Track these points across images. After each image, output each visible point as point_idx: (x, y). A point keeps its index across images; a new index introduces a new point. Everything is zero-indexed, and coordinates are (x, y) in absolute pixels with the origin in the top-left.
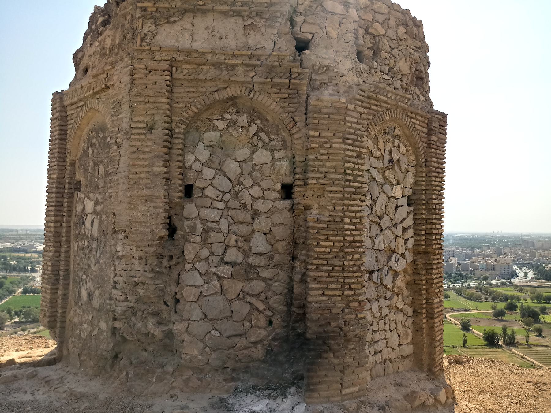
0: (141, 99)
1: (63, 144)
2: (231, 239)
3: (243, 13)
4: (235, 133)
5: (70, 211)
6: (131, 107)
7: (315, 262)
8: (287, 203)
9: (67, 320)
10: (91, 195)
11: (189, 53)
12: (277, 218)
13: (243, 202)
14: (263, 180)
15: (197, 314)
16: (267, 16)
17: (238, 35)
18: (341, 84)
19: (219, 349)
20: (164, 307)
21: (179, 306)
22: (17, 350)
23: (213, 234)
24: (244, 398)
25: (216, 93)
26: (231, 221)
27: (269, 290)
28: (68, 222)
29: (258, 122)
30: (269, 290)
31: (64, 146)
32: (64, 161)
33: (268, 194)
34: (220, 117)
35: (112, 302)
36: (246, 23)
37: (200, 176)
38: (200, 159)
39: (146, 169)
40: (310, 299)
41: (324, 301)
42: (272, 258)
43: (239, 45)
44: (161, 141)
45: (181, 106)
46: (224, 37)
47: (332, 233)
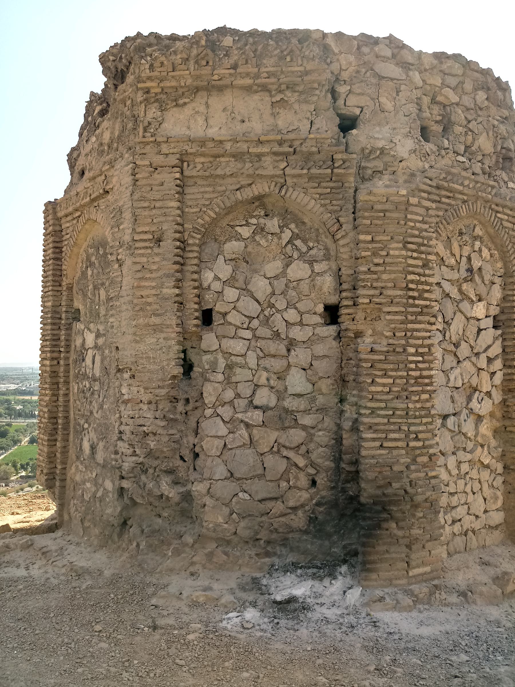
0: (146, 204)
1: (58, 265)
2: (260, 376)
3: (270, 86)
4: (263, 242)
5: (68, 346)
8: (332, 329)
11: (203, 142)
12: (320, 349)
13: (275, 329)
14: (300, 300)
15: (221, 471)
16: (301, 88)
17: (264, 116)
18: (400, 172)
19: (250, 515)
20: (181, 463)
21: (199, 462)
23: (238, 370)
24: (282, 578)
26: (261, 354)
27: (311, 441)
28: (67, 359)
29: (293, 226)
30: (311, 441)
31: (59, 268)
33: (309, 319)
34: (244, 223)
36: (274, 100)
37: (220, 299)
38: (221, 276)
39: (153, 292)
40: (364, 453)
42: (313, 400)
44: (170, 256)
45: (195, 210)
46: (247, 120)
47: (391, 366)
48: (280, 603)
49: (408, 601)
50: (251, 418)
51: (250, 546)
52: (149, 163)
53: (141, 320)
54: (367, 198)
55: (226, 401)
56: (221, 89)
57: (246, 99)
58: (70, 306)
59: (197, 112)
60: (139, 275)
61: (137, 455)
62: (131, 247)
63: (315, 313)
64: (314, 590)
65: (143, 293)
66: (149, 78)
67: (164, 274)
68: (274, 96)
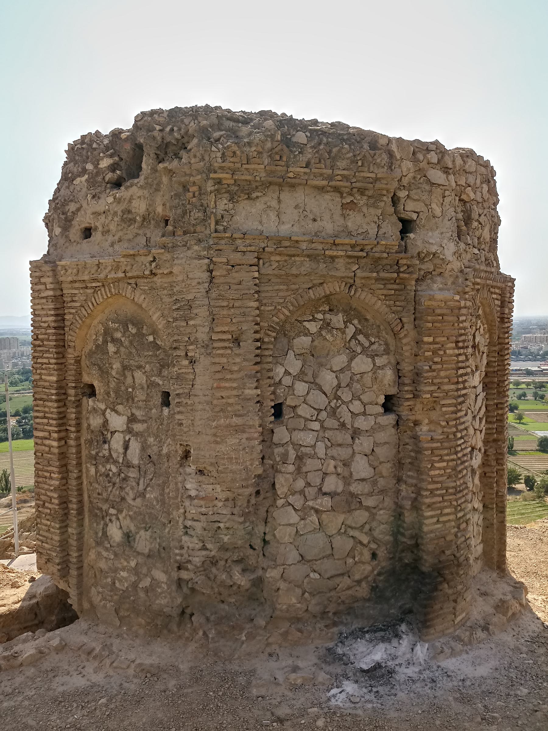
0: (225, 304)
1: (60, 334)
2: (328, 465)
5: (78, 425)
6: (211, 313)
7: (430, 487)
8: (391, 418)
9: (85, 565)
10: (120, 408)
11: (279, 241)
12: (382, 437)
13: (342, 420)
14: (364, 392)
15: (293, 556)
16: (370, 193)
17: (334, 216)
19: (319, 593)
20: (251, 551)
21: (270, 549)
23: (309, 461)
24: (354, 645)
25: (310, 291)
26: (329, 444)
27: (374, 519)
28: (78, 439)
29: (356, 322)
31: (62, 337)
33: (371, 409)
34: (311, 318)
36: (344, 201)
37: (290, 393)
38: (291, 371)
39: (235, 392)
40: (425, 529)
43: (337, 228)
44: (252, 356)
45: (270, 308)
46: (319, 219)
47: (446, 452)
48: (367, 671)
49: (459, 647)
50: (321, 505)
51: (318, 619)
52: (225, 260)
56: (293, 186)
57: (318, 197)
58: (78, 380)
59: (269, 207)
61: (207, 549)
62: (207, 346)
64: (388, 652)
65: (223, 394)
67: (246, 375)
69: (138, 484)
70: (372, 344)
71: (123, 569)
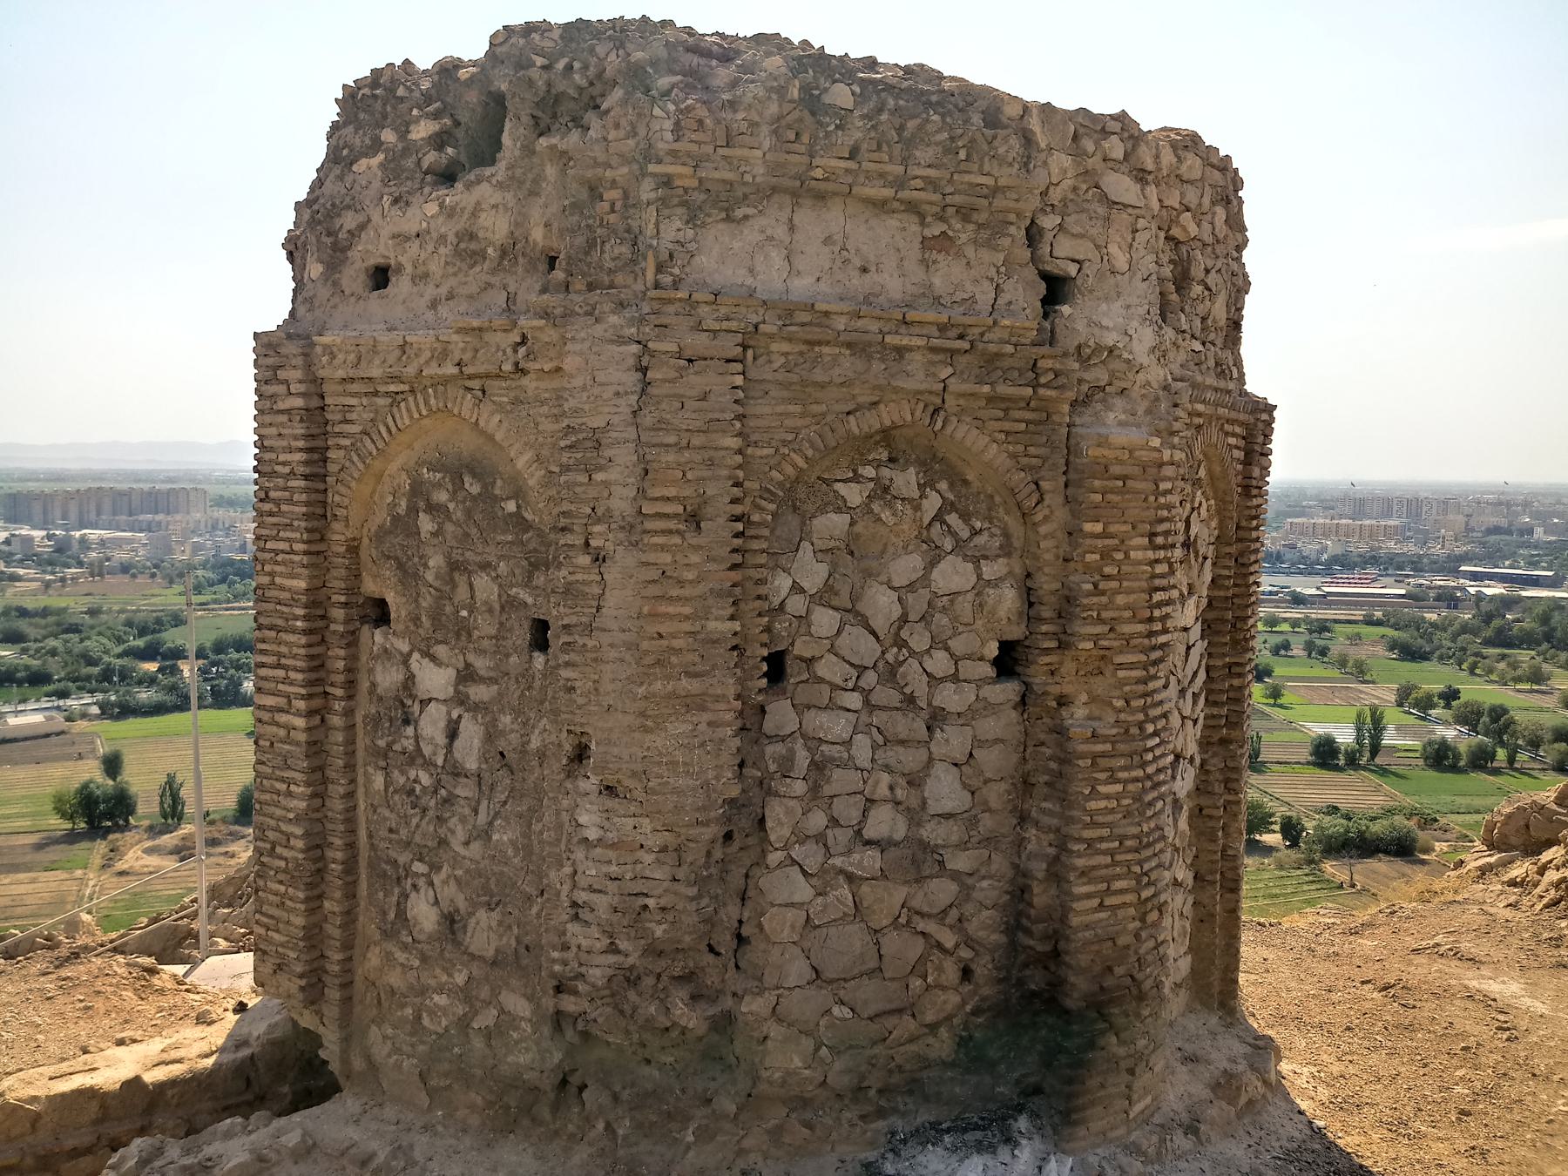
0: (672, 439)
1: (317, 491)
2: (877, 783)
3: (927, 207)
4: (886, 515)
5: (351, 684)
6: (642, 459)
7: (1087, 834)
8: (1008, 691)
9: (358, 979)
10: (441, 651)
11: (788, 312)
12: (990, 727)
13: (907, 690)
14: (956, 634)
15: (798, 970)
16: (982, 217)
17: (906, 263)
18: (1136, 392)
19: (851, 1047)
20: (711, 958)
21: (750, 955)
22: (121, 1043)
24: (920, 1158)
25: (851, 418)
26: (880, 740)
27: (968, 898)
28: (349, 713)
29: (943, 486)
30: (968, 898)
31: (320, 497)
32: (322, 539)
33: (967, 669)
35: (570, 955)
36: (927, 233)
37: (802, 630)
38: (805, 585)
39: (686, 626)
40: (1075, 921)
41: (1101, 920)
42: (973, 822)
43: (910, 289)
45: (766, 451)
46: (873, 269)
47: (1122, 762)
50: (860, 865)
53: (658, 685)
54: (1099, 452)
55: (809, 833)
56: (821, 197)
60: (653, 590)
62: (632, 527)
63: (981, 659)
66: (673, 153)
68: (929, 225)
69: (476, 812)
70: (975, 532)
71: (440, 990)
